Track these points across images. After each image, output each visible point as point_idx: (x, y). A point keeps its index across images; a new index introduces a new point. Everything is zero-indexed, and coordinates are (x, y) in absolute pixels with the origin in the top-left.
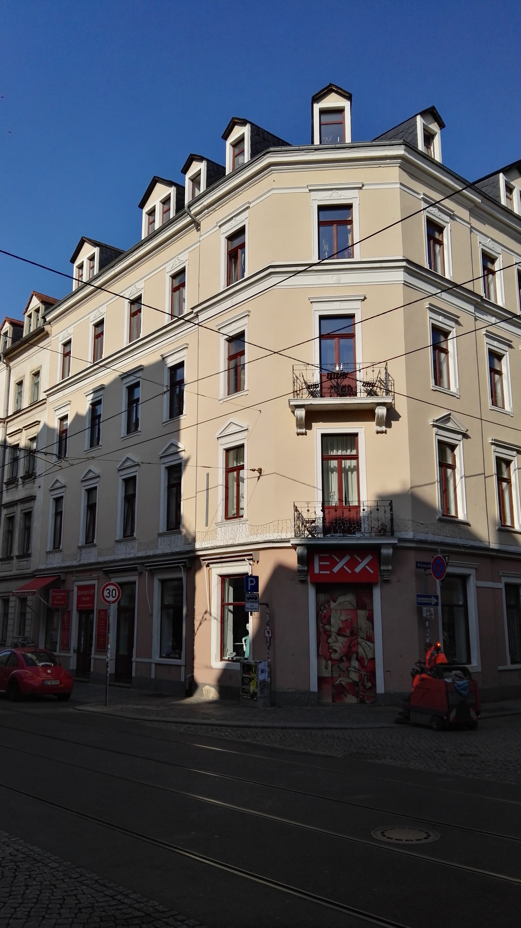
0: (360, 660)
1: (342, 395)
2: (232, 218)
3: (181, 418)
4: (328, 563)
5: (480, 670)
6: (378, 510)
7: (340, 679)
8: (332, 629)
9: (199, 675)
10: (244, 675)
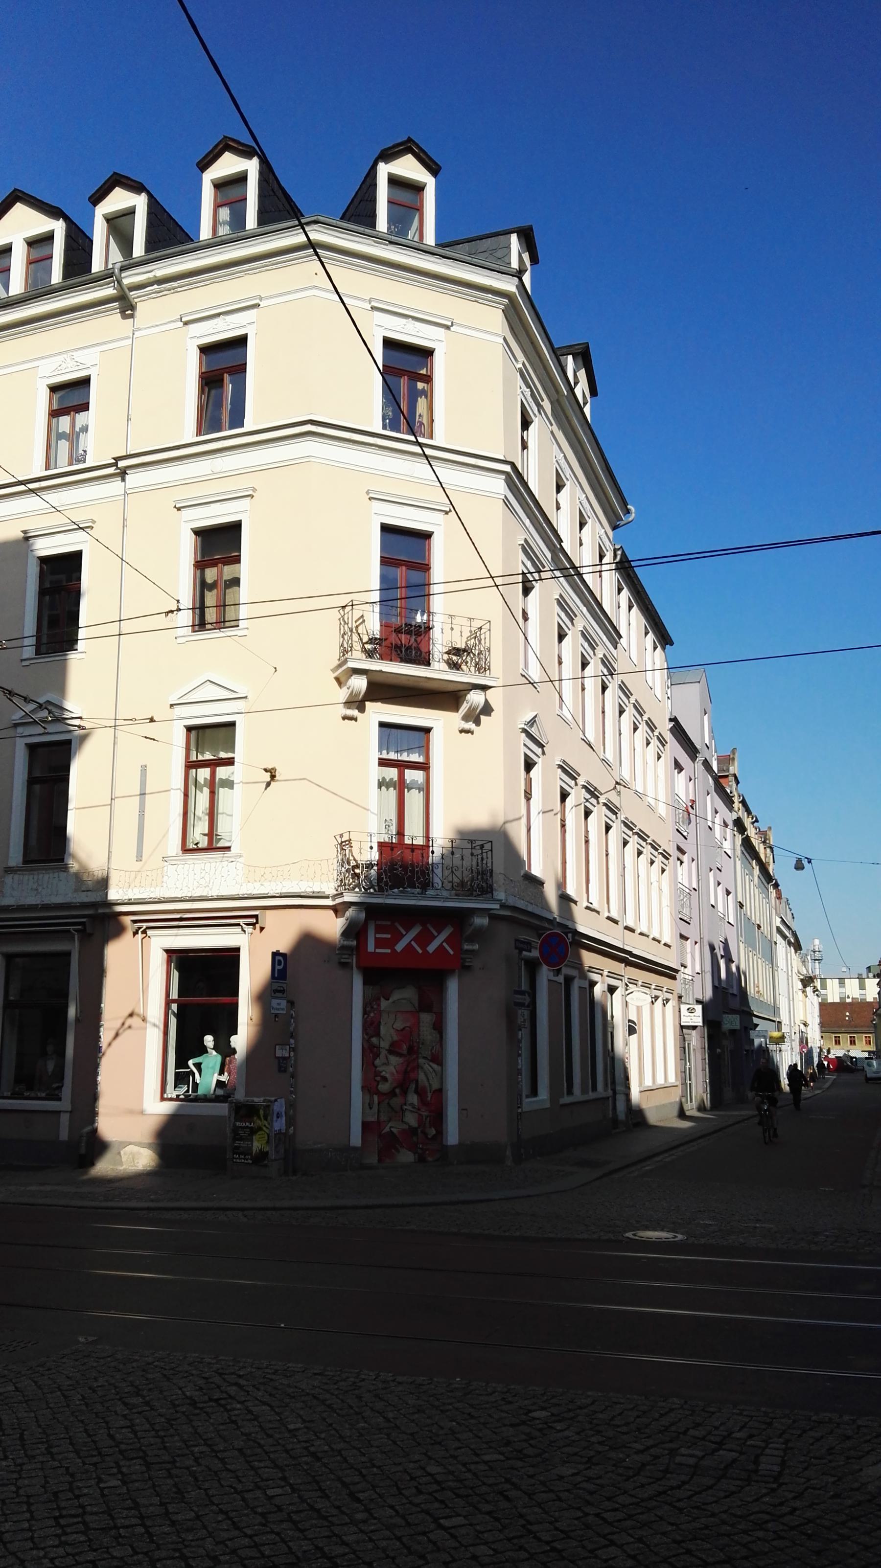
0: (420, 1092)
1: (407, 659)
2: (218, 315)
3: (69, 657)
4: (389, 936)
5: (548, 1105)
6: (453, 853)
7: (389, 1125)
8: (382, 1044)
9: (107, 1125)
10: (238, 1124)
